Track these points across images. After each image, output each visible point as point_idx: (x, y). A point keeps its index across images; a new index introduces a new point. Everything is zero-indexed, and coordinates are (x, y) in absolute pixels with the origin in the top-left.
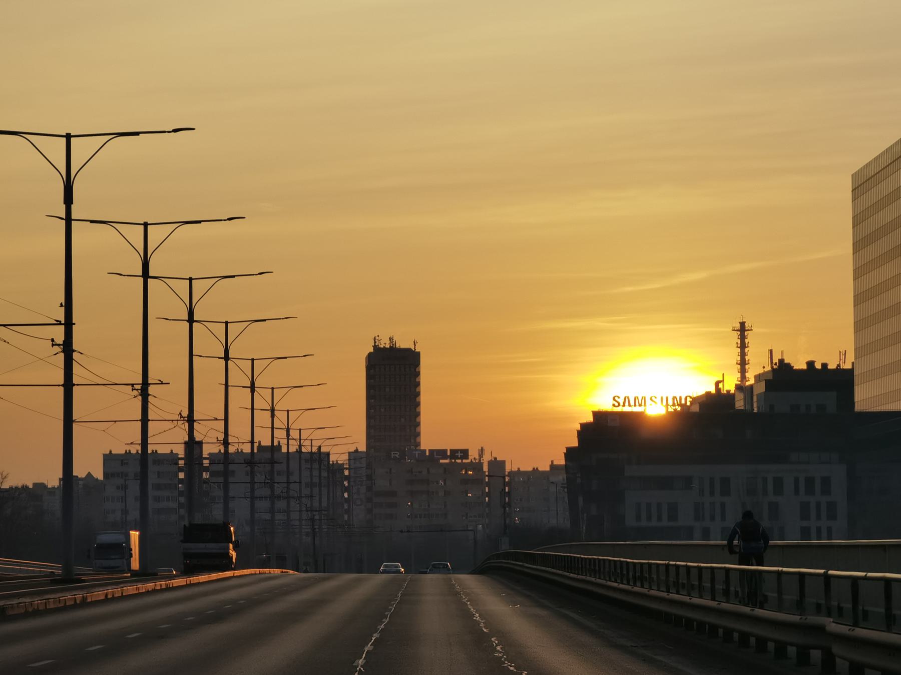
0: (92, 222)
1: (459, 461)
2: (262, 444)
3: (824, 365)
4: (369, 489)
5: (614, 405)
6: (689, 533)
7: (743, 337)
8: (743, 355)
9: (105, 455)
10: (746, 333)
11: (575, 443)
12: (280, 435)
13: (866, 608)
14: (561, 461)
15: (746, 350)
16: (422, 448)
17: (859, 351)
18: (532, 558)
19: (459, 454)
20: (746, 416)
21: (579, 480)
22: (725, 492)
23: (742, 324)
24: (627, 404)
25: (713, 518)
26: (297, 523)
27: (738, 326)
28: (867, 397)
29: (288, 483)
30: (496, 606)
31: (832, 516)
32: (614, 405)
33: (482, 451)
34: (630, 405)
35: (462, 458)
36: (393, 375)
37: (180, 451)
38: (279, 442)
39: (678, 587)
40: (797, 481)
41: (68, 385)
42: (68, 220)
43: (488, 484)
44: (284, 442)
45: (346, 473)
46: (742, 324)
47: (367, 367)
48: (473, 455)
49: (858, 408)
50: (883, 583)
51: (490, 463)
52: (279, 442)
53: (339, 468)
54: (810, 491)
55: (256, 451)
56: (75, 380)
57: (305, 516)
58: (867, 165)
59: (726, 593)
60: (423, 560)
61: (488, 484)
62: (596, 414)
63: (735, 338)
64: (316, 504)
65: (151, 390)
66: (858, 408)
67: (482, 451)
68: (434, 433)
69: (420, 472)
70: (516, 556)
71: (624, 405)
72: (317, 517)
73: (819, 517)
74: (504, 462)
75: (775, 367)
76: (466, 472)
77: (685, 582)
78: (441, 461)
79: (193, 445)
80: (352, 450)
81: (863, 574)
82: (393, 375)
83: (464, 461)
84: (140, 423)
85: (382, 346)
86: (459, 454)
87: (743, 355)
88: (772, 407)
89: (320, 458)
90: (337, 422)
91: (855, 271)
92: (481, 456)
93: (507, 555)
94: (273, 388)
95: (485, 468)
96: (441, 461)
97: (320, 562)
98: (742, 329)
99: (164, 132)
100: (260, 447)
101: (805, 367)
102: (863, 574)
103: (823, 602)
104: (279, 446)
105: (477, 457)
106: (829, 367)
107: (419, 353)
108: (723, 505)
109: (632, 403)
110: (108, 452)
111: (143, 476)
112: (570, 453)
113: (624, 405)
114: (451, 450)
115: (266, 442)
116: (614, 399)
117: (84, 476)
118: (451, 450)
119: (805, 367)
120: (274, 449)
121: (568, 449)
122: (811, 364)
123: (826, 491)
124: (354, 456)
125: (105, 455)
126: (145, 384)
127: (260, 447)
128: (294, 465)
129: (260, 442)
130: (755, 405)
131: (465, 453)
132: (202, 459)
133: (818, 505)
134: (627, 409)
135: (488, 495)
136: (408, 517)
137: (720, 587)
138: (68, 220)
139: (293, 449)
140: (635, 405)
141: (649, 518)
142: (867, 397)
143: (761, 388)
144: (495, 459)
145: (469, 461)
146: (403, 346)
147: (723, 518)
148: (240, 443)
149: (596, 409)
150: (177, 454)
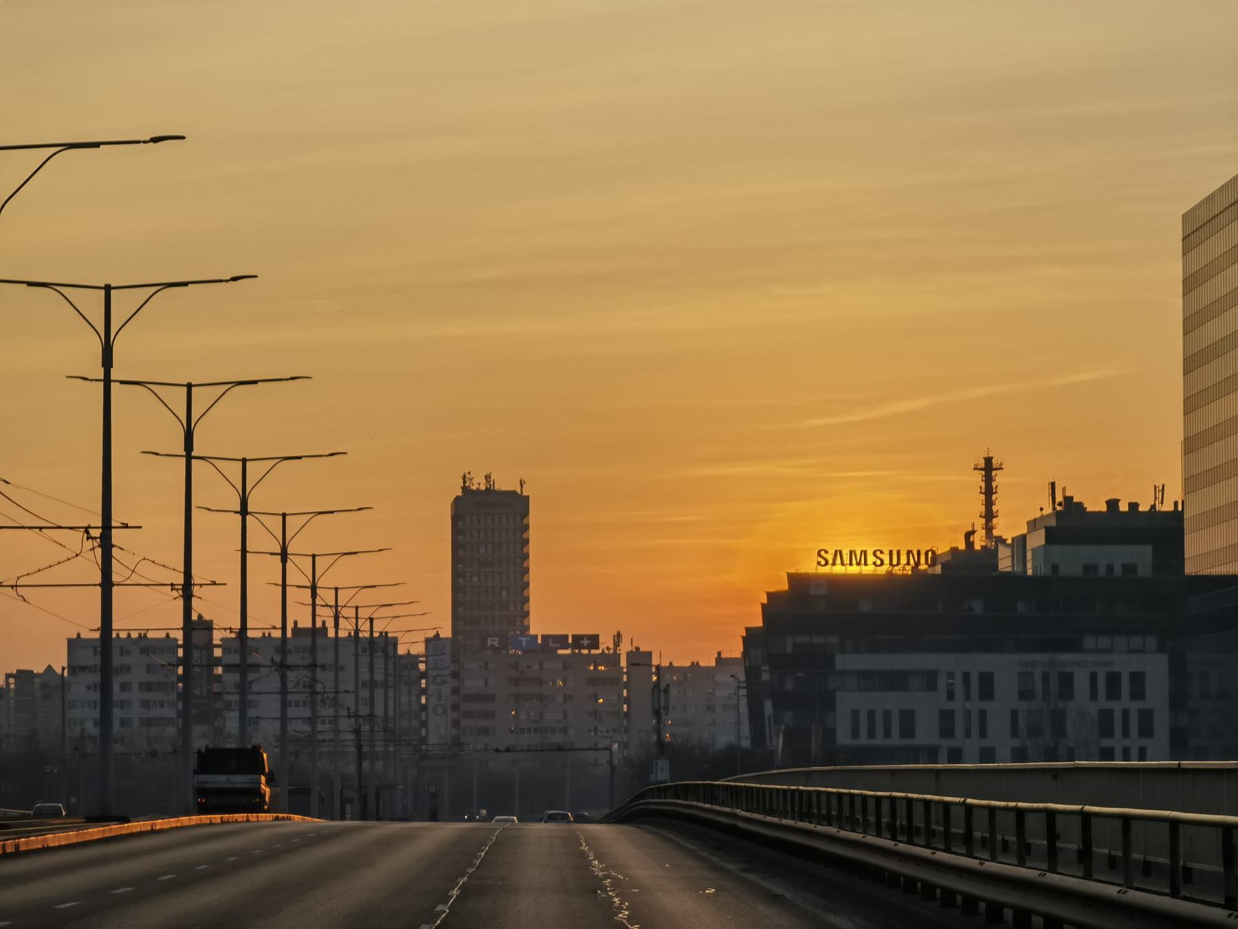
0: (30, 284)
1: (585, 652)
2: (300, 625)
3: (1133, 506)
4: (455, 691)
5: (819, 563)
6: (932, 755)
7: (989, 480)
8: (989, 504)
9: (69, 641)
10: (994, 473)
11: (758, 622)
12: (325, 615)
13: (1189, 865)
14: (735, 650)
15: (994, 497)
16: (532, 632)
17: (1190, 484)
18: (710, 794)
19: (586, 642)
20: (1015, 581)
21: (766, 677)
22: (987, 692)
23: (988, 460)
24: (838, 561)
25: (968, 734)
26: (351, 736)
27: (982, 464)
28: (1203, 554)
29: (313, 666)
30: (621, 850)
31: (1146, 730)
32: (819, 563)
33: (618, 638)
34: (842, 564)
35: (589, 647)
36: (489, 529)
37: (179, 636)
38: (324, 622)
39: (910, 834)
40: (1093, 677)
41: (107, 584)
42: (107, 381)
43: (627, 685)
44: (330, 623)
45: (422, 667)
46: (988, 460)
47: (453, 519)
48: (606, 642)
49: (1189, 569)
50: (1044, 815)
51: (629, 654)
52: (324, 622)
53: (412, 660)
54: (1114, 693)
55: (289, 635)
56: (115, 578)
57: (344, 724)
58: (1210, 199)
59: (1085, 857)
60: (538, 801)
61: (627, 685)
62: (793, 579)
63: (978, 479)
64: (364, 711)
65: (117, 536)
66: (1189, 569)
67: (618, 638)
68: (546, 616)
69: (529, 667)
70: (683, 792)
71: (834, 564)
72: (366, 728)
73: (1126, 733)
74: (650, 653)
75: (1058, 508)
76: (595, 668)
77: (922, 825)
78: (560, 652)
79: (196, 628)
80: (431, 634)
81: (1003, 804)
82: (489, 529)
83: (593, 651)
84: (99, 589)
85: (474, 488)
86: (586, 642)
87: (989, 504)
88: (1055, 568)
89: (387, 644)
90: (415, 604)
91: (1186, 361)
92: (617, 643)
93: (663, 791)
94: (284, 515)
95: (623, 663)
96: (560, 652)
97: (369, 803)
98: (988, 468)
99: (138, 142)
100: (296, 629)
101: (1104, 508)
102: (1003, 804)
103: (1120, 854)
104: (325, 628)
105: (611, 646)
106: (1141, 509)
107: (527, 498)
108: (983, 714)
109: (846, 560)
110: (75, 636)
111: (106, 669)
112: (751, 638)
113: (834, 564)
114: (573, 636)
115: (306, 623)
116: (819, 555)
117: (41, 671)
118: (573, 636)
119: (1104, 508)
120: (316, 633)
121: (747, 629)
122: (1113, 504)
123: (1138, 694)
124: (433, 642)
125: (69, 641)
126: (107, 526)
127: (296, 629)
128: (346, 657)
129: (296, 623)
130: (1029, 565)
131: (594, 641)
132: (210, 646)
133: (1126, 713)
134: (839, 569)
135: (627, 700)
136: (512, 732)
137: (901, 821)
138: (107, 381)
139: (346, 629)
140: (851, 564)
141: (871, 733)
142: (1203, 554)
143: (1037, 540)
144: (638, 649)
145: (599, 651)
146: (504, 488)
147: (983, 734)
148: (264, 620)
149: (793, 571)
150: (176, 640)
